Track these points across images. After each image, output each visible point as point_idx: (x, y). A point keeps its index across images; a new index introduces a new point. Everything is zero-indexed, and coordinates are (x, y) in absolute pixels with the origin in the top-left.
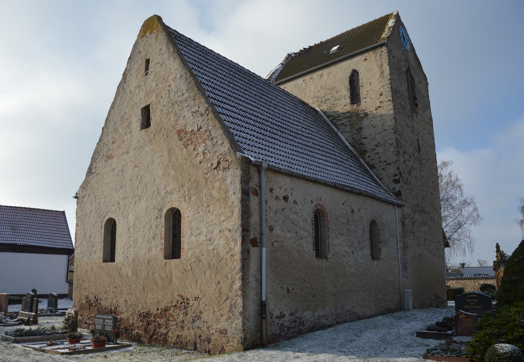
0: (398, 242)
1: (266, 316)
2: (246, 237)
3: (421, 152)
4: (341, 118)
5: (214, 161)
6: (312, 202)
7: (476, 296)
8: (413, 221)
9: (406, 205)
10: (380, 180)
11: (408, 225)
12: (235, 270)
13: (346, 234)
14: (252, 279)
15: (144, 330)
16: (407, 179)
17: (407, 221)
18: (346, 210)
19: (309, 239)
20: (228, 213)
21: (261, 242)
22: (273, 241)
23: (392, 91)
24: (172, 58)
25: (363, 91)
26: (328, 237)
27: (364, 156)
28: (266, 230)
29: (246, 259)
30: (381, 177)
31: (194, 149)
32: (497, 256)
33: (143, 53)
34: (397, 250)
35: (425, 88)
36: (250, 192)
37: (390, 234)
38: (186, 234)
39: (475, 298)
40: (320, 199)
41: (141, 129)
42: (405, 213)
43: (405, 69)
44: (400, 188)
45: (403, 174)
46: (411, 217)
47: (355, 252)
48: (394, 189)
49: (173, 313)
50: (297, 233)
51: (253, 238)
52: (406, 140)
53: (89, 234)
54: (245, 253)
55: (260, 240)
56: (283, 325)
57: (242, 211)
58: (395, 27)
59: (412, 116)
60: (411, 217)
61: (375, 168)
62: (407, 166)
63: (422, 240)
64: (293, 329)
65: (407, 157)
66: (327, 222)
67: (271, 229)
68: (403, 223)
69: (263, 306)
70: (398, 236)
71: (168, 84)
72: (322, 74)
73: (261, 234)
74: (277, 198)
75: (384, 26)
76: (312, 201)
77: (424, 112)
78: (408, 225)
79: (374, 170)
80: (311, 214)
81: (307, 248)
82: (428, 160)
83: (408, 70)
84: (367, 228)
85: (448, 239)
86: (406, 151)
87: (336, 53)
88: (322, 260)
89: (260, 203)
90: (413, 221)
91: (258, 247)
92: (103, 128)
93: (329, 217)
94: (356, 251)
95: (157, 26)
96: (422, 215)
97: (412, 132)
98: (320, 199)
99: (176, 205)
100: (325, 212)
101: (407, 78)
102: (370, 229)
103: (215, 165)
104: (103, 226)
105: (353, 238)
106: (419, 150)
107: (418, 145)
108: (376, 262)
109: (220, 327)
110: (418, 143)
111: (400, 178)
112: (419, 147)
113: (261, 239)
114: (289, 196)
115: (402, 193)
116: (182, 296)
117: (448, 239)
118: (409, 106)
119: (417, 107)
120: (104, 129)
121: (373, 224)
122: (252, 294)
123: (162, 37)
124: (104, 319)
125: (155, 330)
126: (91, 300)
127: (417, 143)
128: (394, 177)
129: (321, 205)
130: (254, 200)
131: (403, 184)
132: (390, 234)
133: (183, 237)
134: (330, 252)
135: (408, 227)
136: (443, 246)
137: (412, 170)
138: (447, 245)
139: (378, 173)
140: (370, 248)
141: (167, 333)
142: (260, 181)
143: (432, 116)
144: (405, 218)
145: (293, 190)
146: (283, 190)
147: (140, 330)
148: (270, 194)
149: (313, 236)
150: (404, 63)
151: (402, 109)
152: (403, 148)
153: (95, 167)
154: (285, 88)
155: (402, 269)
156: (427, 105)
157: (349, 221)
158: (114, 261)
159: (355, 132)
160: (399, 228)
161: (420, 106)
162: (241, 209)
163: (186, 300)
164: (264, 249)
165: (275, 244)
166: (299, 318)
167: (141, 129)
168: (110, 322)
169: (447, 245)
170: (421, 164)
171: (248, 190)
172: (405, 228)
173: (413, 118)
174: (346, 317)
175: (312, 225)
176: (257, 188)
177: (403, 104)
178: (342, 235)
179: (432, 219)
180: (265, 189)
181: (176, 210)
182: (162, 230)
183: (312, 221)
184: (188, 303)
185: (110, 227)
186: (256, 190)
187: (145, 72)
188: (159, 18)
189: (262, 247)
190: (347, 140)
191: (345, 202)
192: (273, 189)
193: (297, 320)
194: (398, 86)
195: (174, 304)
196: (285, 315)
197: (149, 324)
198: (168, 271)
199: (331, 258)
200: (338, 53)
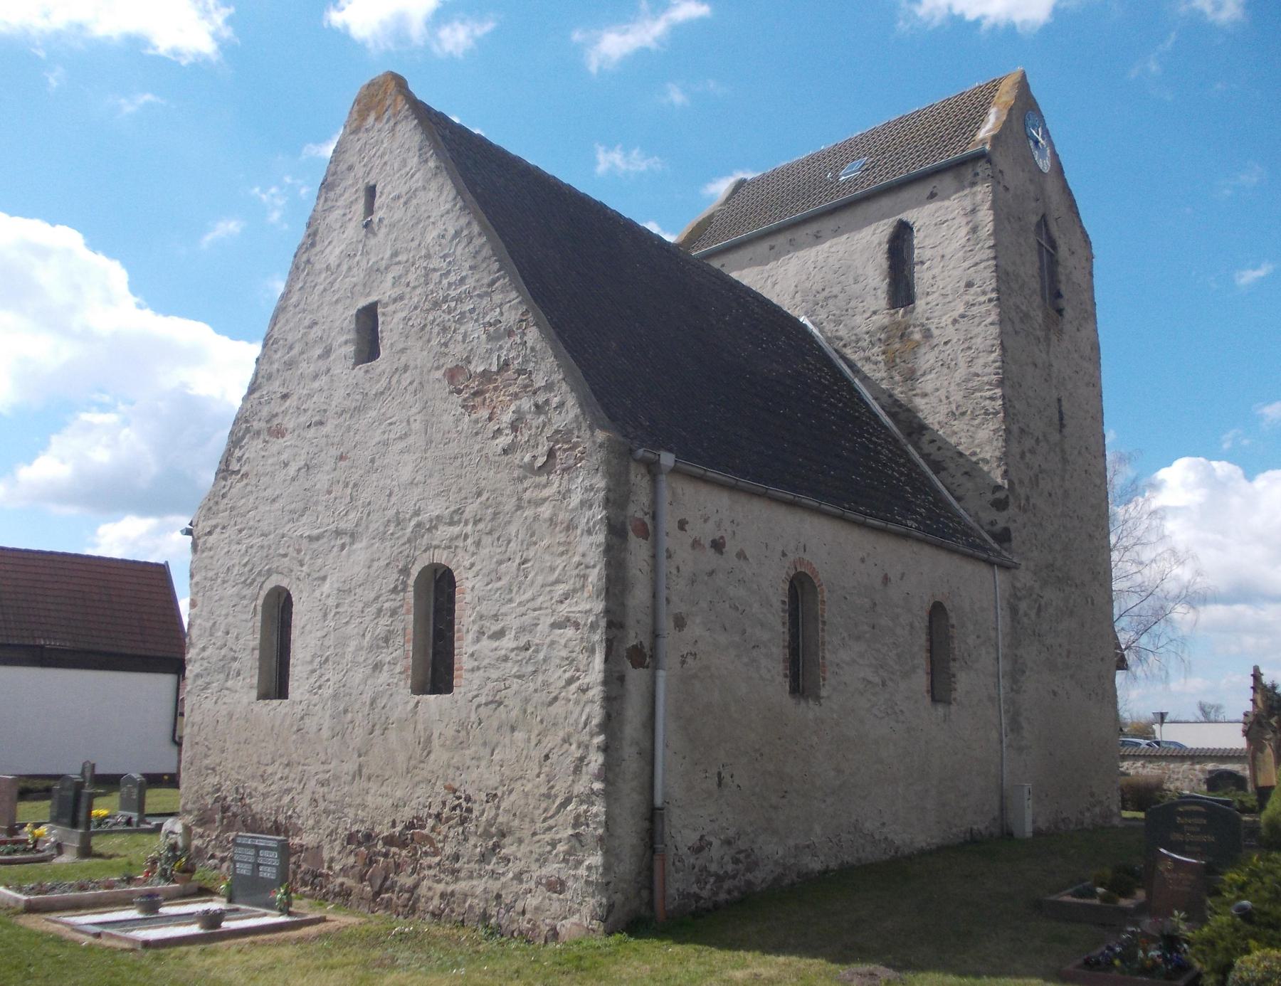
0: (998, 658)
1: (663, 846)
2: (615, 644)
3: (1066, 431)
4: (865, 344)
5: (540, 447)
6: (784, 555)
7: (1203, 810)
8: (1040, 606)
9: (1023, 563)
10: (958, 499)
11: (1026, 615)
12: (588, 727)
13: (868, 635)
14: (629, 753)
15: (358, 876)
16: (1027, 499)
17: (1023, 606)
18: (869, 575)
19: (774, 650)
20: (572, 581)
21: (654, 656)
22: (685, 653)
23: (998, 276)
24: (434, 185)
25: (922, 277)
26: (823, 644)
27: (919, 438)
28: (667, 624)
29: (615, 698)
30: (959, 492)
31: (490, 419)
32: (1254, 701)
33: (359, 170)
34: (996, 680)
35: (1084, 268)
36: (629, 528)
37: (978, 637)
38: (468, 632)
39: (1198, 814)
40: (805, 546)
41: (356, 364)
42: (1018, 585)
43: (1034, 219)
44: (1007, 522)
45: (1017, 486)
46: (1034, 596)
47: (890, 683)
48: (993, 523)
49: (434, 835)
50: (744, 632)
51: (633, 646)
52: (1029, 400)
53: (223, 628)
54: (614, 681)
55: (651, 650)
56: (706, 871)
57: (608, 576)
58: (1014, 112)
59: (1048, 339)
60: (1034, 596)
61: (944, 469)
62: (1028, 466)
63: (1060, 654)
64: (731, 880)
65: (1028, 443)
66: (820, 606)
67: (680, 623)
68: (1014, 611)
69: (653, 816)
70: (1000, 645)
71: (423, 252)
72: (818, 232)
73: (655, 635)
74: (696, 544)
75: (985, 109)
76: (783, 552)
77: (1078, 330)
78: (1026, 615)
79: (943, 474)
80: (782, 585)
81: (769, 671)
82: (1083, 450)
83: (1043, 223)
84: (921, 623)
85: (1126, 649)
86: (1027, 429)
87: (856, 180)
88: (807, 702)
89: (654, 556)
90: (1040, 606)
91: (647, 667)
92: (258, 359)
93: (826, 594)
94: (891, 680)
95: (395, 100)
96: (1064, 591)
97: (1045, 379)
98: (805, 546)
99: (443, 559)
100: (815, 581)
101: (1038, 241)
102: (928, 624)
103: (540, 461)
104: (259, 609)
105: (886, 648)
106: (1062, 426)
107: (1061, 413)
108: (941, 710)
109: (548, 875)
110: (1060, 406)
111: (1010, 497)
112: (1061, 419)
113: (654, 648)
114: (726, 539)
115: (1013, 535)
116: (455, 791)
117: (1126, 649)
118: (1040, 315)
119: (1061, 315)
120: (261, 360)
121: (937, 611)
122: (631, 797)
123: (409, 133)
124: (257, 848)
125: (386, 879)
126: (225, 798)
127: (1057, 407)
128: (994, 493)
129: (806, 562)
130: (638, 551)
131: (1017, 510)
132: (978, 637)
133: (460, 639)
134: (826, 682)
135: (1025, 620)
136: (1115, 667)
137: (1040, 475)
138: (1122, 664)
139: (953, 484)
140: (927, 673)
141: (416, 886)
142: (654, 502)
143: (1100, 339)
144: (1020, 599)
145: (738, 525)
146: (711, 524)
147: (348, 876)
148: (679, 534)
149: (784, 641)
150: (1034, 204)
151: (1022, 321)
152: (1020, 419)
153: (239, 459)
154: (723, 266)
155: (1008, 729)
156: (1086, 312)
157: (875, 604)
158: (286, 697)
159: (897, 378)
160: (1003, 623)
161: (1069, 313)
162: (604, 573)
163: (465, 800)
164: (661, 674)
165: (690, 660)
166: (746, 850)
167: (356, 364)
168: (272, 857)
169: (1122, 664)
170: (1065, 461)
171: (623, 524)
172: (1019, 623)
173: (1049, 345)
174: (863, 851)
175: (782, 614)
176: (647, 519)
177: (1024, 308)
178: (858, 638)
179: (1089, 600)
180: (668, 522)
181: (443, 570)
182: (408, 619)
183: (784, 602)
184: (469, 810)
185: (277, 610)
186: (644, 524)
187: (365, 218)
188: (400, 83)
189: (656, 668)
190: (876, 399)
191: (868, 554)
192: (687, 523)
193: (742, 856)
194: (1014, 263)
195: (434, 811)
196: (711, 844)
197: (371, 861)
198: (420, 727)
199: (828, 697)
200: (862, 177)
